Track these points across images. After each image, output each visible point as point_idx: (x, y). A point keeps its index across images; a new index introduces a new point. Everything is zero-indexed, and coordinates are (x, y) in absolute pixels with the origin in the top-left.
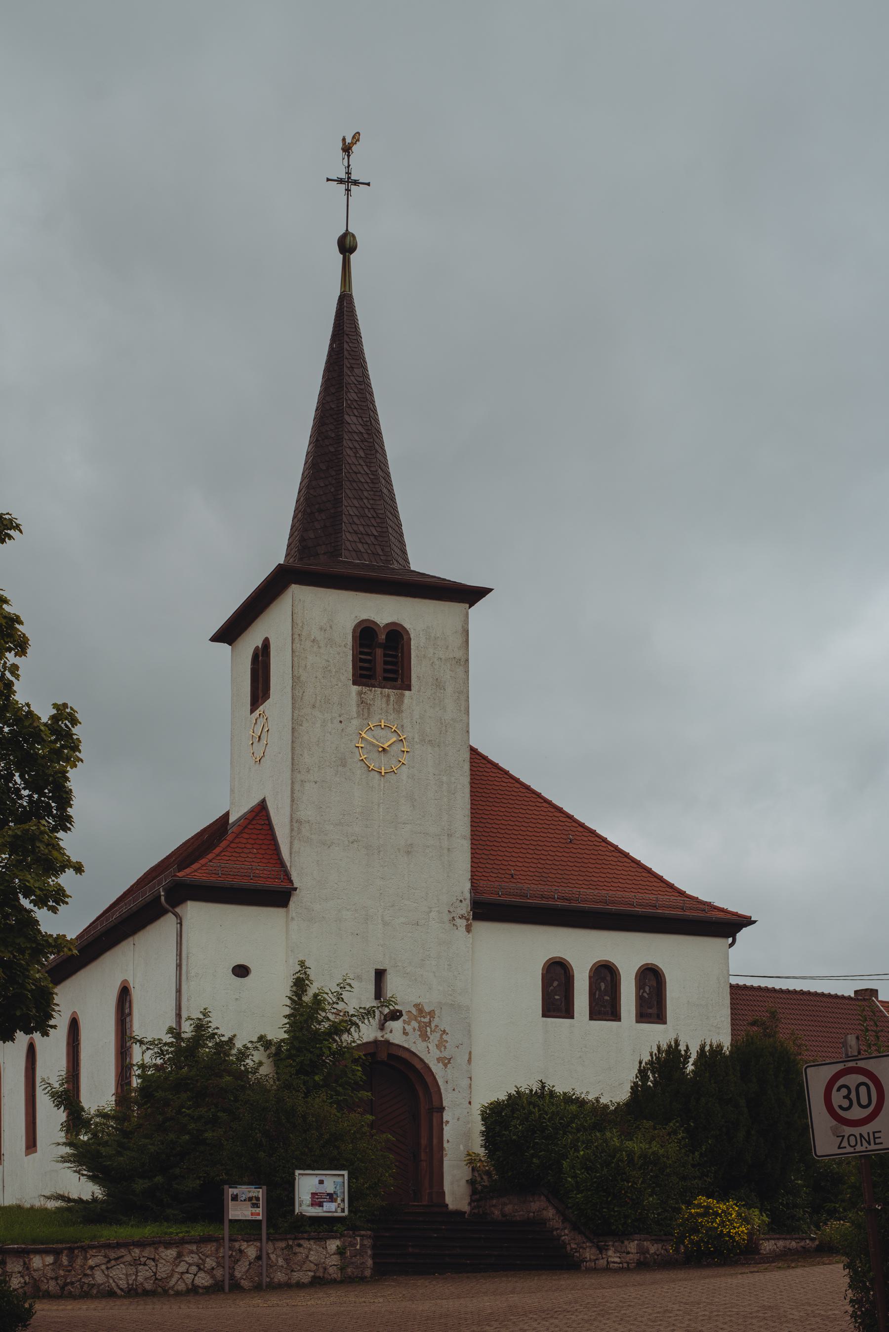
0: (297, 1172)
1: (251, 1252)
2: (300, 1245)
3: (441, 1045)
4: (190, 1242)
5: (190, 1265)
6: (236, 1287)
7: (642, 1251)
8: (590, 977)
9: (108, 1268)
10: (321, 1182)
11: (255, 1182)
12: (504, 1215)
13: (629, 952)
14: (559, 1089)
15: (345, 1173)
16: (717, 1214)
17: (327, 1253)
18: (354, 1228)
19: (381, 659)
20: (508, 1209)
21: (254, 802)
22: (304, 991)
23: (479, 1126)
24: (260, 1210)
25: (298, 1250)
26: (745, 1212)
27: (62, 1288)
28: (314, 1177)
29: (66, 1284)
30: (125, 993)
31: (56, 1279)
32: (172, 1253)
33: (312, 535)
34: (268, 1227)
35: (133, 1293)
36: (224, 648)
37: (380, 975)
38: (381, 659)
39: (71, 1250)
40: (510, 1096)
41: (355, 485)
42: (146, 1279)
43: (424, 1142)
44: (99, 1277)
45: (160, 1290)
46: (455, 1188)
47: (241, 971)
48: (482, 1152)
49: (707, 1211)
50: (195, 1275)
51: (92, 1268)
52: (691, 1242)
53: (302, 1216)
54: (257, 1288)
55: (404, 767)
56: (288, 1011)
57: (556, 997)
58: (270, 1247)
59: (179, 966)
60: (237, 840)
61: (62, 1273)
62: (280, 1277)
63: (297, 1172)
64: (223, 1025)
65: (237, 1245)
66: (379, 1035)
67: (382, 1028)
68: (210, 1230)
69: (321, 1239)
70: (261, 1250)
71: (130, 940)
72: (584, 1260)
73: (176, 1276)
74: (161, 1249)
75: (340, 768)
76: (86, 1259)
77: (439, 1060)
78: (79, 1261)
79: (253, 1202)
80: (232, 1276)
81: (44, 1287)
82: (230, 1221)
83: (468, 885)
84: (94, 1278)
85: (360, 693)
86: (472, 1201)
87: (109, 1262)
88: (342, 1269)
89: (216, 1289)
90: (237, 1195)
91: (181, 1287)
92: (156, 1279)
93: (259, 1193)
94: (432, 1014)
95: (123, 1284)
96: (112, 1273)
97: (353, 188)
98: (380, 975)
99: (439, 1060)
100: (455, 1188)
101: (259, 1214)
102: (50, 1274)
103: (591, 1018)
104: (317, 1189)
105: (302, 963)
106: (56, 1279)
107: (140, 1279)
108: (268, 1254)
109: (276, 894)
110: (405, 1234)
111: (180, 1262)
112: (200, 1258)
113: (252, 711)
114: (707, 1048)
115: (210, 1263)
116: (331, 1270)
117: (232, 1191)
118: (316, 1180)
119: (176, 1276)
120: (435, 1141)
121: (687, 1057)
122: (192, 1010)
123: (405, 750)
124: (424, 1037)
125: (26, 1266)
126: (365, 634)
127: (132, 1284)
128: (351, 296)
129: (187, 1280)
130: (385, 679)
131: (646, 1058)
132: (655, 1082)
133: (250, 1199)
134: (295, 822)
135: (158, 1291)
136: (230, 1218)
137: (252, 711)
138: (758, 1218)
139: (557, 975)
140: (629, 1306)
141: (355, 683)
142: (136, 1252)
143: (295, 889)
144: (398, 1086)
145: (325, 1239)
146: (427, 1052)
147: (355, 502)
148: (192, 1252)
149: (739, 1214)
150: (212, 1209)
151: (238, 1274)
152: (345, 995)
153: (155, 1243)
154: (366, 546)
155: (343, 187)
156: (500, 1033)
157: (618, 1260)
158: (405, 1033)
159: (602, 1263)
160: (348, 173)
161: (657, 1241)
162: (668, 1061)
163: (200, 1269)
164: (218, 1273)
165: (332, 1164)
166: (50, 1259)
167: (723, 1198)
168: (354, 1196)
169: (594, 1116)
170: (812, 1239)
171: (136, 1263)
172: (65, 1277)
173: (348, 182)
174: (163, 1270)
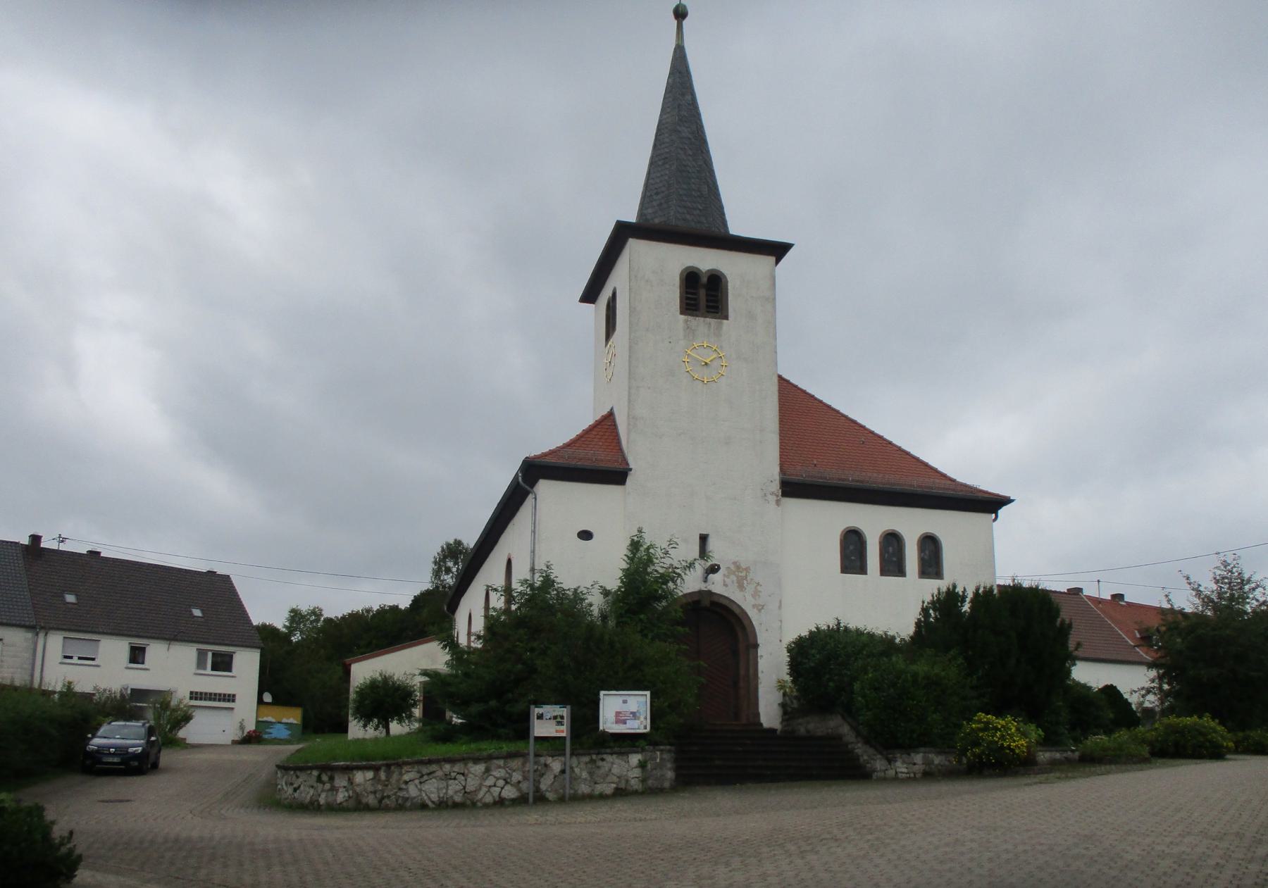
0: (602, 693)
1: (556, 765)
2: (603, 760)
3: (756, 594)
4: (498, 758)
5: (498, 779)
6: (540, 799)
7: (927, 762)
10: (625, 702)
11: (561, 702)
12: (808, 731)
13: (912, 524)
14: (852, 626)
16: (996, 729)
18: (655, 744)
19: (703, 296)
20: (811, 726)
22: (638, 550)
23: (785, 657)
24: (564, 728)
25: (600, 763)
26: (1023, 727)
27: (380, 802)
29: (383, 798)
30: (509, 562)
31: (375, 792)
32: (480, 768)
33: (650, 211)
34: (572, 744)
35: (444, 805)
37: (704, 539)
38: (703, 296)
39: (388, 766)
40: (811, 632)
42: (456, 792)
43: (742, 672)
44: (413, 791)
45: (468, 802)
46: (769, 712)
47: (586, 535)
48: (788, 678)
49: (986, 727)
51: (406, 783)
52: (974, 754)
53: (604, 732)
54: (562, 800)
56: (625, 566)
57: (852, 552)
58: (574, 761)
59: (534, 532)
61: (380, 787)
62: (584, 789)
63: (602, 693)
64: (567, 580)
65: (542, 760)
66: (703, 587)
67: (705, 580)
68: (520, 746)
69: (623, 754)
72: (874, 771)
73: (484, 789)
74: (470, 765)
76: (401, 774)
77: (754, 606)
78: (395, 776)
79: (558, 720)
80: (537, 790)
81: (364, 800)
82: (537, 739)
83: (777, 469)
85: (686, 321)
86: (783, 720)
87: (422, 776)
88: (644, 781)
89: (521, 801)
91: (488, 799)
93: (565, 712)
94: (747, 569)
95: (434, 797)
96: (426, 787)
98: (704, 539)
99: (754, 606)
100: (769, 712)
101: (563, 731)
102: (370, 788)
103: (882, 574)
104: (625, 710)
105: (640, 531)
106: (375, 792)
107: (450, 792)
108: (572, 768)
109: (617, 476)
110: (712, 745)
114: (981, 591)
115: (517, 777)
116: (633, 782)
117: (537, 711)
118: (620, 699)
119: (484, 789)
120: (751, 671)
121: (964, 598)
122: (540, 565)
124: (741, 587)
125: (351, 781)
126: (691, 279)
131: (928, 599)
132: (936, 618)
133: (555, 718)
134: (632, 418)
135: (465, 805)
138: (1035, 733)
139: (853, 544)
140: (912, 831)
141: (682, 313)
142: (447, 767)
144: (718, 627)
145: (627, 754)
146: (744, 600)
149: (1018, 729)
150: (521, 729)
151: (543, 787)
152: (671, 551)
153: (463, 760)
156: (802, 584)
157: (905, 770)
158: (726, 585)
159: (891, 773)
161: (939, 753)
162: (948, 601)
163: (507, 783)
164: (525, 786)
165: (637, 685)
166: (370, 775)
167: (999, 713)
168: (656, 715)
169: (887, 645)
170: (1073, 751)
171: (447, 777)
172: (383, 791)
174: (472, 784)
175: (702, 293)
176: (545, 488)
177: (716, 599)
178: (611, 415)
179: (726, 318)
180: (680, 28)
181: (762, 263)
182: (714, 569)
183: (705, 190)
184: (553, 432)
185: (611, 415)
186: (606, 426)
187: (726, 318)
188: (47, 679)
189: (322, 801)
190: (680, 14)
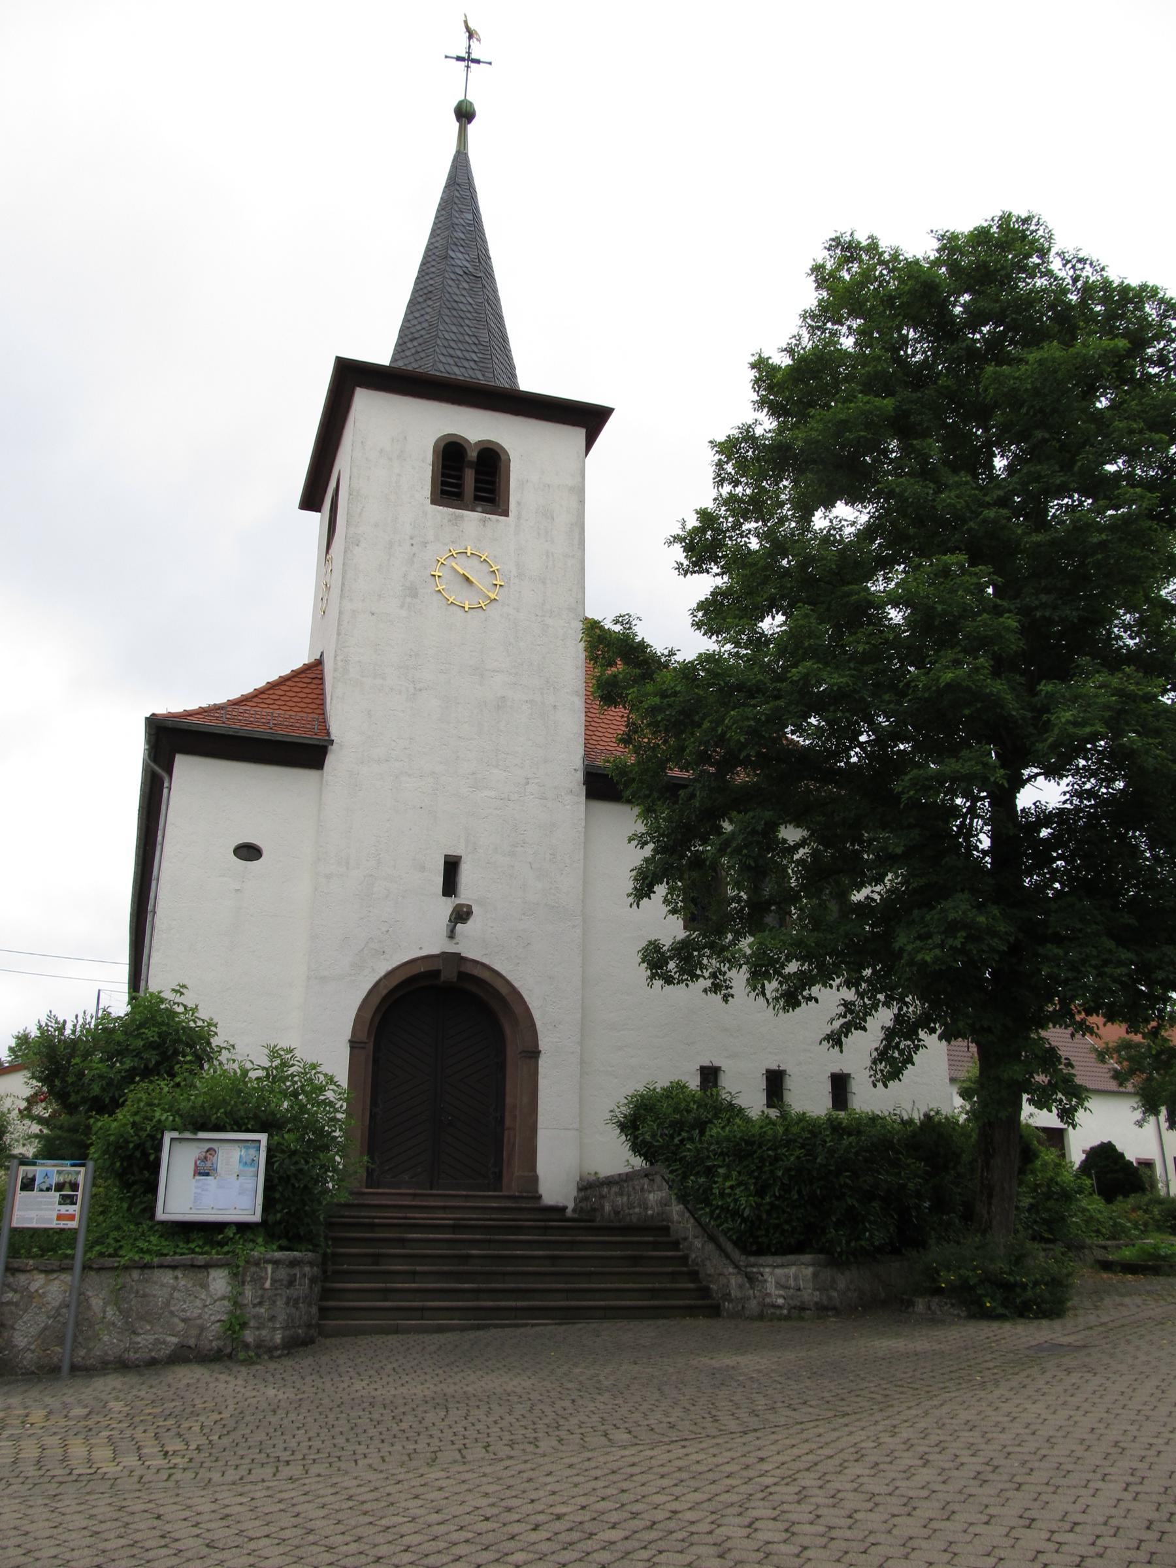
15: (263, 1137)
19: (470, 479)
28: (195, 1144)
37: (452, 867)
38: (470, 479)
41: (454, 313)
60: (271, 692)
62: (109, 1342)
66: (451, 948)
75: (408, 600)
79: (66, 1191)
90: (33, 1179)
97: (473, 65)
98: (452, 867)
109: (308, 753)
123: (498, 582)
128: (466, 154)
130: (477, 498)
133: (60, 1187)
136: (15, 1224)
141: (433, 502)
147: (454, 329)
154: (463, 370)
155: (473, 56)
160: (469, 53)
173: (468, 60)
175: (469, 476)
177: (468, 969)
178: (319, 663)
179: (506, 513)
183: (484, 336)
185: (319, 663)
186: (308, 681)
187: (506, 513)
190: (465, 114)
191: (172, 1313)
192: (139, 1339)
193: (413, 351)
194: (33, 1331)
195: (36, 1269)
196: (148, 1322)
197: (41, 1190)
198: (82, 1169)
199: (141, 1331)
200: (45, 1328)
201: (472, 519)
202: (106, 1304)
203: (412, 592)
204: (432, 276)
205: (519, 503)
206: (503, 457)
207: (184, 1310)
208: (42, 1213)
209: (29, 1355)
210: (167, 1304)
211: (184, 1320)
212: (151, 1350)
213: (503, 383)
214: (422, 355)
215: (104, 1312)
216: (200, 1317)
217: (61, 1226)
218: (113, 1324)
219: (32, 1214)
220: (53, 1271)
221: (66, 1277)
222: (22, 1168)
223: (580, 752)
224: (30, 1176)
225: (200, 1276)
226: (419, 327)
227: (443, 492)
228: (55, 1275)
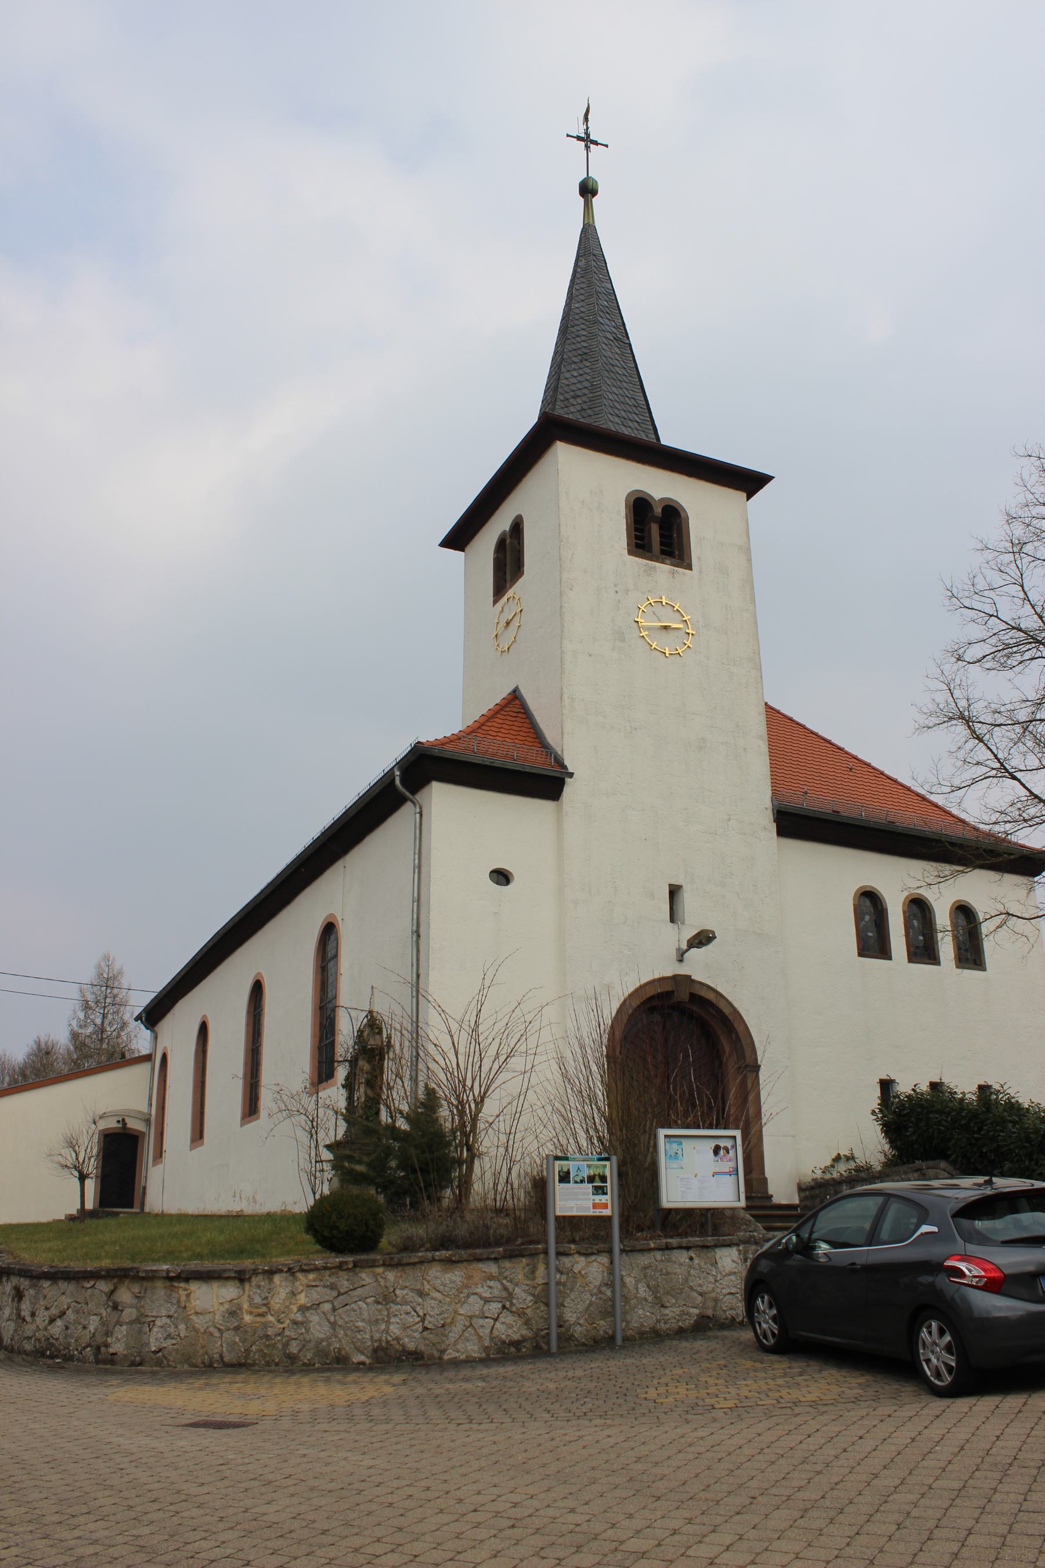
5: (487, 1301)
8: (904, 912)
9: (334, 1309)
13: (946, 889)
17: (718, 1272)
19: (657, 533)
21: (504, 692)
36: (459, 554)
37: (674, 892)
38: (657, 533)
50: (496, 1320)
55: (689, 650)
62: (643, 1316)
63: (662, 1132)
66: (682, 970)
70: (611, 1272)
71: (339, 865)
84: (308, 1331)
90: (568, 1173)
91: (472, 1349)
92: (425, 1329)
95: (367, 1336)
98: (674, 892)
109: (545, 782)
111: (468, 1296)
112: (506, 1289)
113: (495, 602)
126: (640, 508)
127: (380, 1340)
129: (481, 1332)
130: (663, 552)
133: (591, 1179)
136: (558, 1213)
137: (495, 602)
143: (571, 775)
148: (491, 1278)
155: (583, 144)
166: (228, 1292)
169: (561, 440)
173: (587, 140)
175: (655, 529)
176: (443, 800)
180: (588, 208)
181: (733, 497)
182: (702, 939)
184: (443, 717)
188: (450, 988)
189: (118, 1346)
190: (588, 190)
191: (691, 1288)
192: (667, 1311)
193: (579, 408)
194: (581, 1307)
195: (579, 1253)
196: (673, 1296)
197: (576, 1182)
198: (607, 1163)
199: (668, 1304)
200: (591, 1304)
201: (663, 570)
202: (638, 1281)
203: (621, 636)
204: (583, 338)
205: (699, 558)
206: (682, 515)
207: (700, 1285)
208: (578, 1202)
209: (578, 1329)
210: (686, 1280)
211: (701, 1294)
212: (678, 1321)
213: (652, 438)
214: (590, 412)
215: (637, 1289)
216: (713, 1290)
217: (597, 1214)
218: (645, 1299)
219: (572, 1204)
220: (592, 1254)
221: (604, 1259)
222: (557, 1163)
223: (769, 793)
224: (565, 1170)
225: (709, 1255)
226: (579, 386)
227: (638, 546)
228: (593, 1258)
